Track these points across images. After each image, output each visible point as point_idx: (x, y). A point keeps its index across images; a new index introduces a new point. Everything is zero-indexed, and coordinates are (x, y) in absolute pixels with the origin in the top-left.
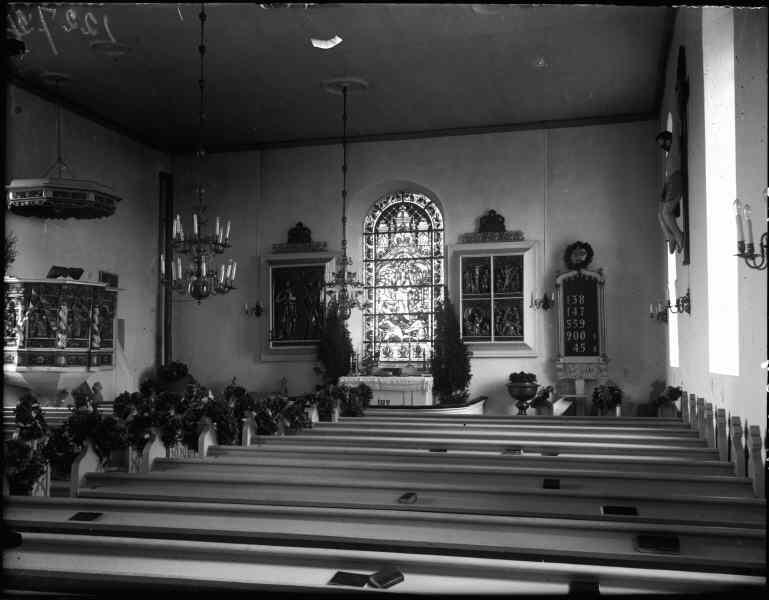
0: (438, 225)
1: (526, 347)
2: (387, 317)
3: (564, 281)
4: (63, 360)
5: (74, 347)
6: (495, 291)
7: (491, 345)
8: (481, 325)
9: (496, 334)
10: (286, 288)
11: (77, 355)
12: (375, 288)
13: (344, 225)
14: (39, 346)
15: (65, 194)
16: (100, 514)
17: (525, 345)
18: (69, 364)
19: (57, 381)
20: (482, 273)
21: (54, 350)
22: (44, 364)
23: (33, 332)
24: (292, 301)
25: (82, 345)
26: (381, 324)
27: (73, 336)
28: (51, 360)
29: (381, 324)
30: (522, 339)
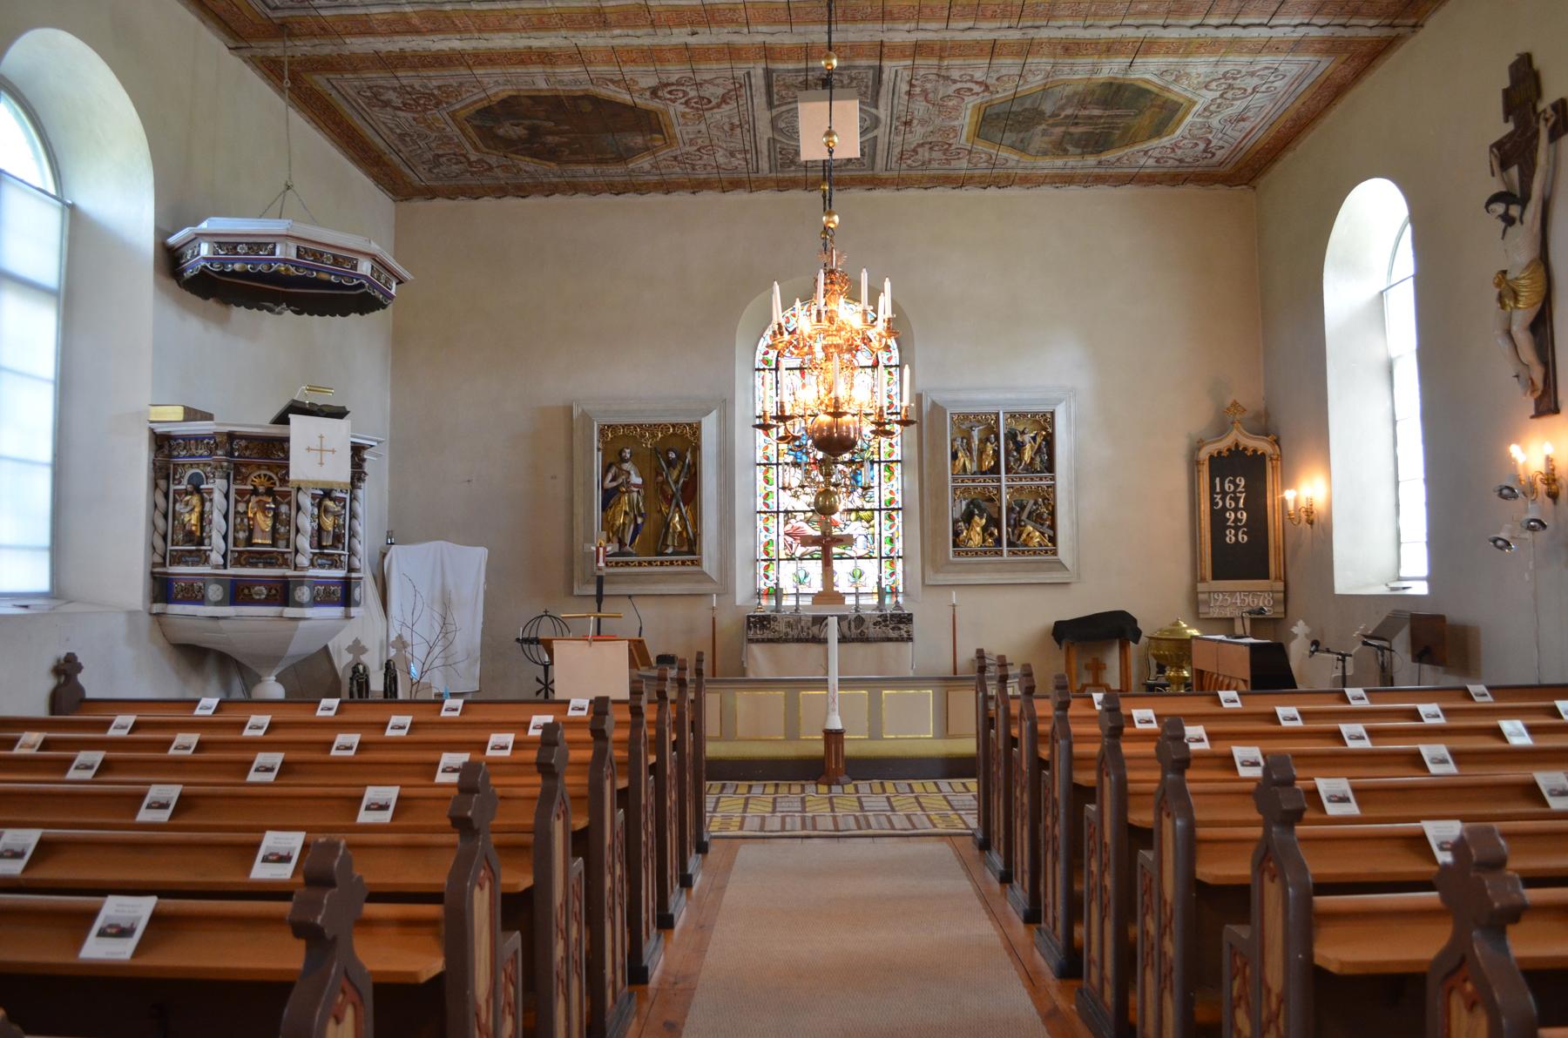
0: (889, 359)
1: (1061, 566)
2: (800, 516)
3: (1211, 457)
4: (214, 592)
5: (322, 566)
6: (1008, 470)
7: (1004, 562)
8: (985, 529)
9: (1010, 544)
10: (624, 460)
11: (326, 582)
12: (778, 464)
13: (29, 376)
14: (254, 565)
15: (318, 256)
16: (1231, 946)
17: (1060, 562)
18: (316, 602)
19: (291, 637)
20: (984, 441)
21: (289, 572)
22: (267, 602)
23: (242, 535)
24: (636, 485)
25: (334, 564)
26: (789, 527)
27: (320, 546)
28: (282, 593)
29: (789, 527)
30: (1055, 553)
